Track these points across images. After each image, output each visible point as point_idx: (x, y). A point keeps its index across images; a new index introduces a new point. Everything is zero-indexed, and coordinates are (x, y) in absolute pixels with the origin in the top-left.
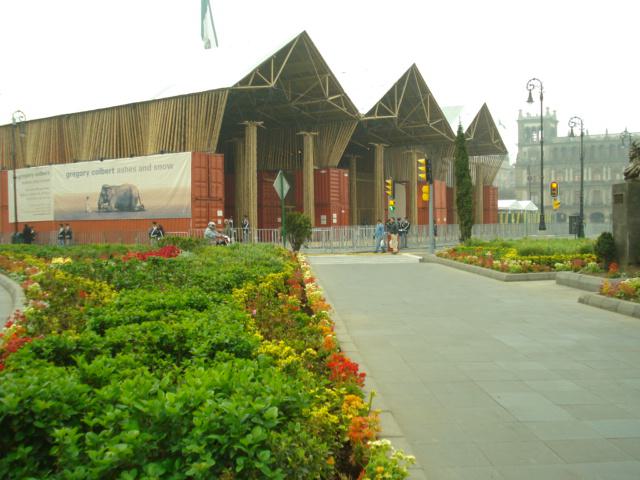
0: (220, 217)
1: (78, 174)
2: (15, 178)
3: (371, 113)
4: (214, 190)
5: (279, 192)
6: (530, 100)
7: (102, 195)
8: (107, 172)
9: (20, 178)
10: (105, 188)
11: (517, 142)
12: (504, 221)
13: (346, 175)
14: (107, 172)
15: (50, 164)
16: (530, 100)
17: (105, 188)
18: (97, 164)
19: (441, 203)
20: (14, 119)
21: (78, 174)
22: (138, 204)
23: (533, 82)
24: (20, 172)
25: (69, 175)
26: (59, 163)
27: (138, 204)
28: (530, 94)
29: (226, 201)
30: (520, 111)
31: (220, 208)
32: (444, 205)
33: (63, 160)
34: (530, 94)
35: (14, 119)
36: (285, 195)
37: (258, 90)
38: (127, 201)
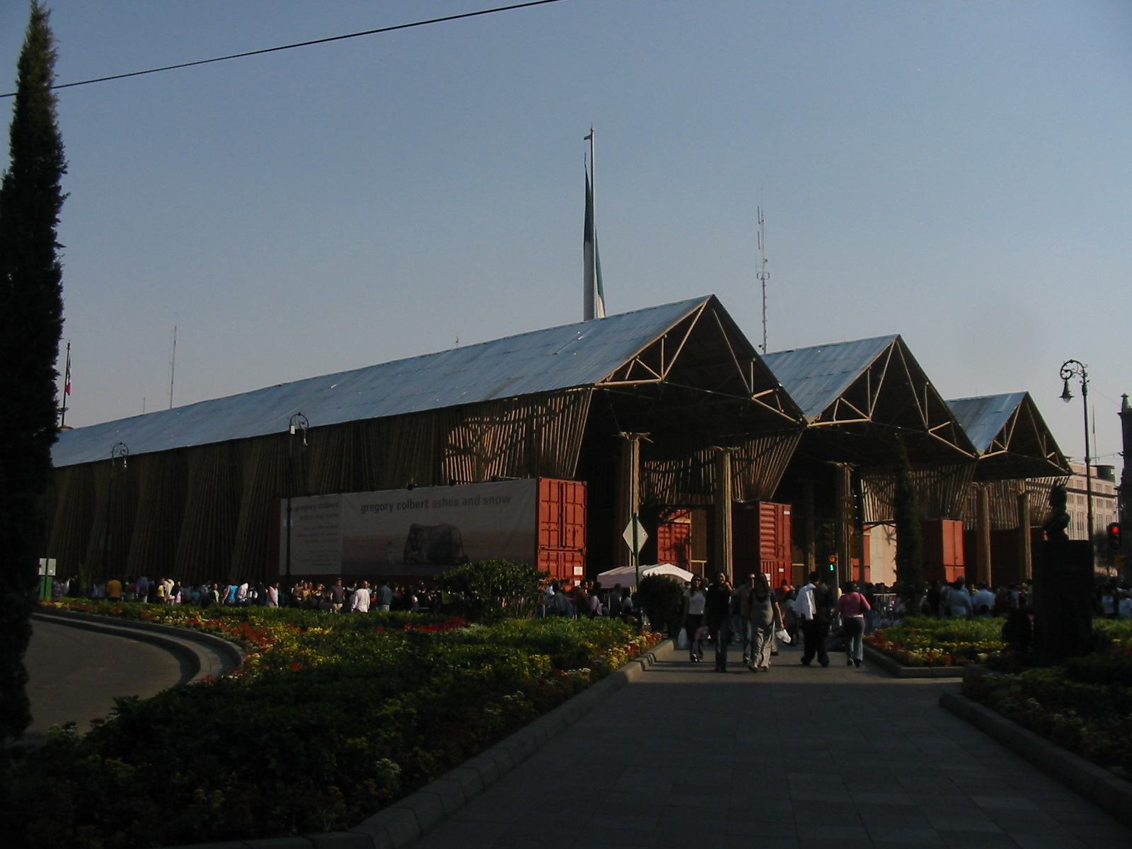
0: (578, 577)
1: (377, 508)
2: (289, 510)
3: (827, 415)
4: (570, 535)
5: (630, 543)
6: (1066, 395)
7: (410, 539)
8: (418, 505)
9: (297, 510)
10: (415, 530)
11: (1121, 450)
12: (632, 565)
13: (787, 513)
14: (418, 505)
15: (339, 491)
16: (1066, 395)
17: (415, 530)
18: (402, 494)
19: (955, 558)
20: (60, 246)
21: (377, 508)
22: (460, 555)
23: (1069, 366)
24: (297, 502)
25: (364, 509)
26: (354, 491)
27: (460, 555)
28: (1066, 384)
29: (587, 552)
30: (1125, 397)
31: (580, 563)
32: (960, 561)
33: (358, 488)
34: (1066, 384)
35: (60, 246)
36: (639, 549)
37: (640, 386)
38: (40, 566)
